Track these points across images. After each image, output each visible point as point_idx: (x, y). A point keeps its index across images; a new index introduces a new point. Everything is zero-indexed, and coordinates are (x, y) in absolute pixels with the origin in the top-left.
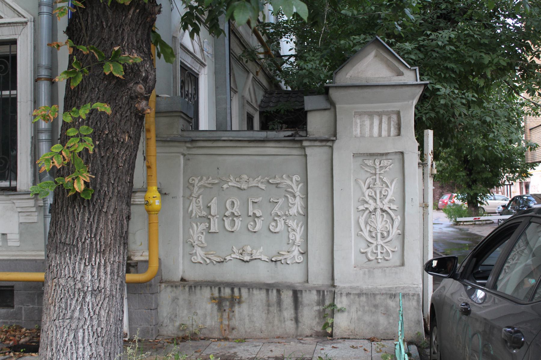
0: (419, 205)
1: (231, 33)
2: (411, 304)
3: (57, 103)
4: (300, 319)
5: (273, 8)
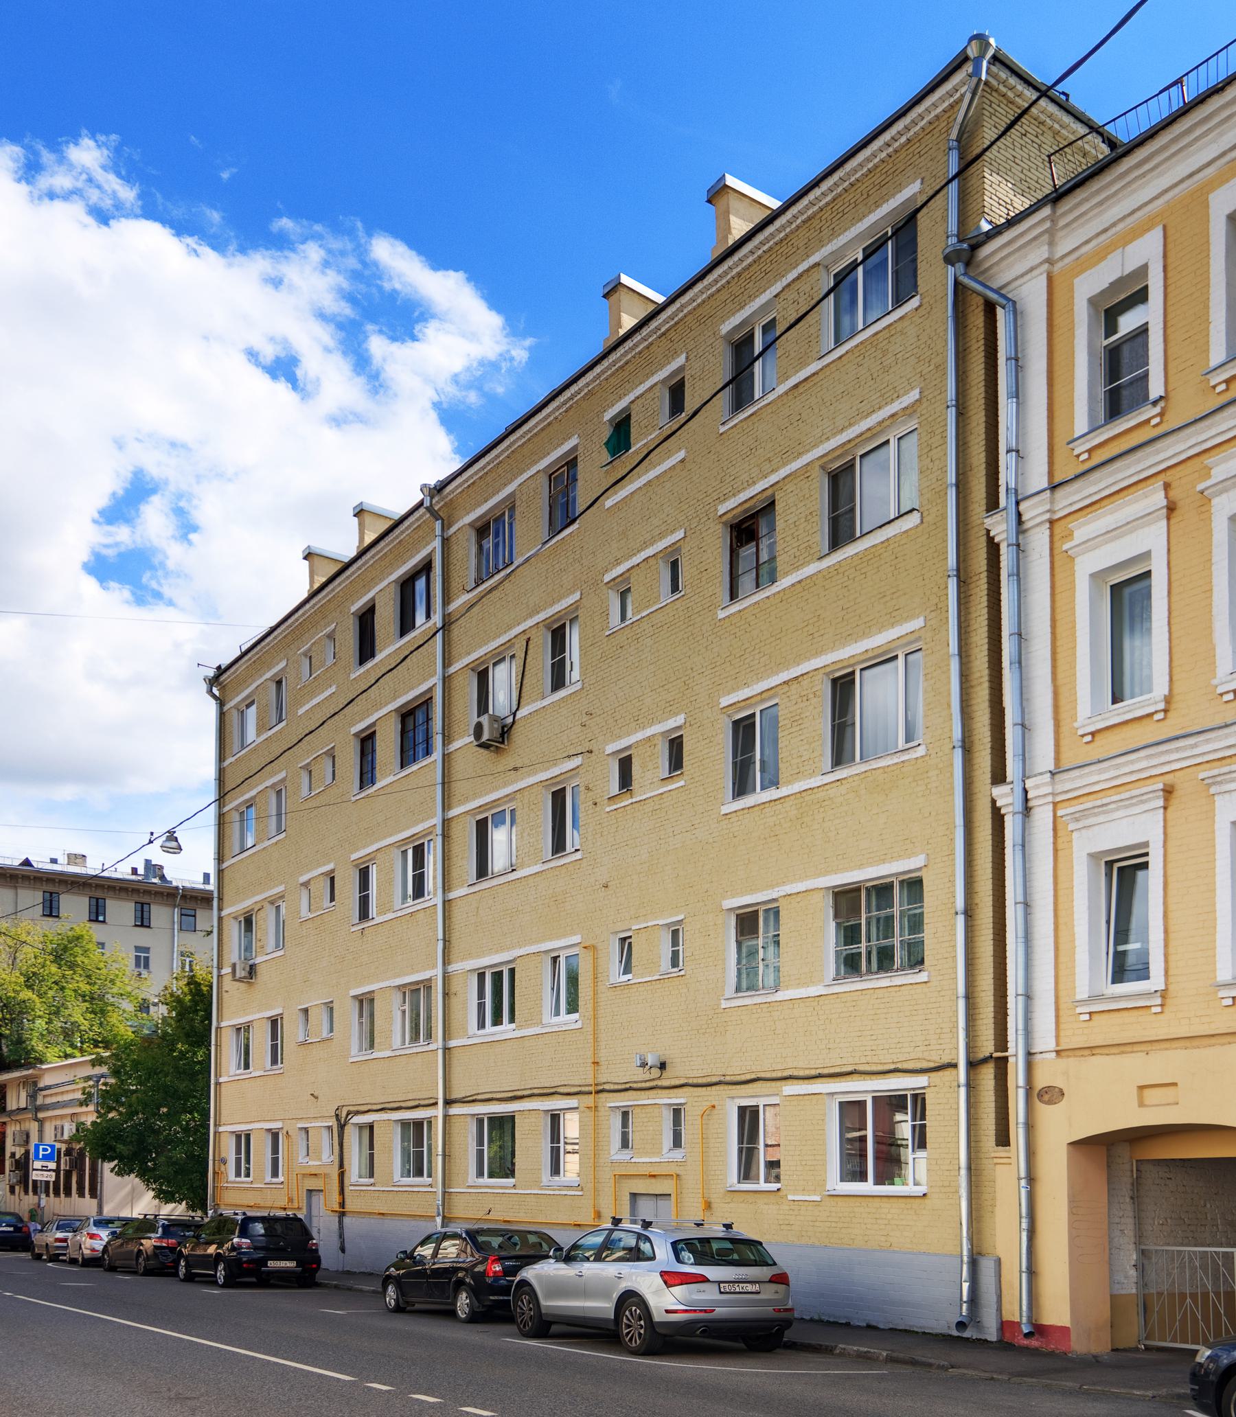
0: (84, 556)
1: (970, 157)
2: (1010, 809)
3: (696, 1263)
4: (1066, 204)
5: (456, 1298)
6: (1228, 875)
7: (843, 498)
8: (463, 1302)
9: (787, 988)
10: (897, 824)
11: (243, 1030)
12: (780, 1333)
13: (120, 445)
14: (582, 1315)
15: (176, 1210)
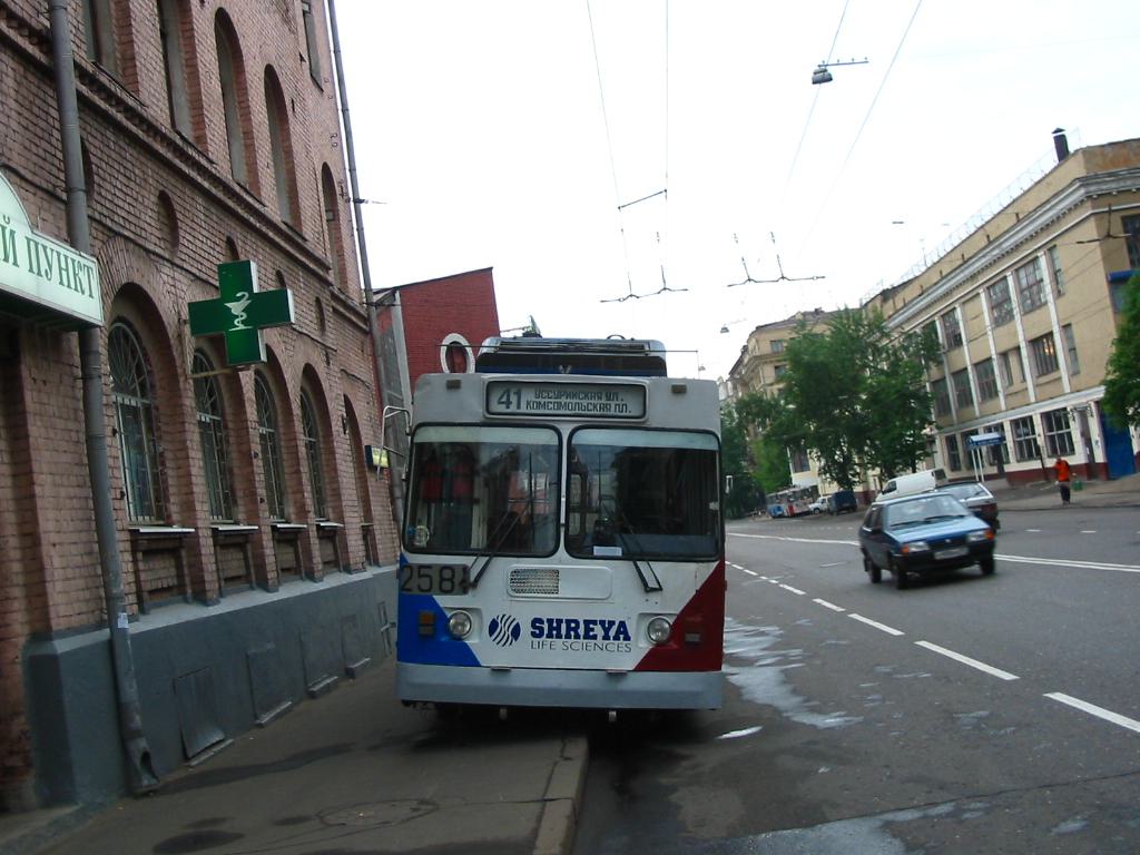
0: (462, 385)
6: (1003, 672)
7: (284, 175)
8: (146, 503)
9: (392, 572)
10: (949, 475)
11: (372, 558)
12: (934, 360)
13: (1077, 129)
14: (70, 313)
15: (1063, 458)
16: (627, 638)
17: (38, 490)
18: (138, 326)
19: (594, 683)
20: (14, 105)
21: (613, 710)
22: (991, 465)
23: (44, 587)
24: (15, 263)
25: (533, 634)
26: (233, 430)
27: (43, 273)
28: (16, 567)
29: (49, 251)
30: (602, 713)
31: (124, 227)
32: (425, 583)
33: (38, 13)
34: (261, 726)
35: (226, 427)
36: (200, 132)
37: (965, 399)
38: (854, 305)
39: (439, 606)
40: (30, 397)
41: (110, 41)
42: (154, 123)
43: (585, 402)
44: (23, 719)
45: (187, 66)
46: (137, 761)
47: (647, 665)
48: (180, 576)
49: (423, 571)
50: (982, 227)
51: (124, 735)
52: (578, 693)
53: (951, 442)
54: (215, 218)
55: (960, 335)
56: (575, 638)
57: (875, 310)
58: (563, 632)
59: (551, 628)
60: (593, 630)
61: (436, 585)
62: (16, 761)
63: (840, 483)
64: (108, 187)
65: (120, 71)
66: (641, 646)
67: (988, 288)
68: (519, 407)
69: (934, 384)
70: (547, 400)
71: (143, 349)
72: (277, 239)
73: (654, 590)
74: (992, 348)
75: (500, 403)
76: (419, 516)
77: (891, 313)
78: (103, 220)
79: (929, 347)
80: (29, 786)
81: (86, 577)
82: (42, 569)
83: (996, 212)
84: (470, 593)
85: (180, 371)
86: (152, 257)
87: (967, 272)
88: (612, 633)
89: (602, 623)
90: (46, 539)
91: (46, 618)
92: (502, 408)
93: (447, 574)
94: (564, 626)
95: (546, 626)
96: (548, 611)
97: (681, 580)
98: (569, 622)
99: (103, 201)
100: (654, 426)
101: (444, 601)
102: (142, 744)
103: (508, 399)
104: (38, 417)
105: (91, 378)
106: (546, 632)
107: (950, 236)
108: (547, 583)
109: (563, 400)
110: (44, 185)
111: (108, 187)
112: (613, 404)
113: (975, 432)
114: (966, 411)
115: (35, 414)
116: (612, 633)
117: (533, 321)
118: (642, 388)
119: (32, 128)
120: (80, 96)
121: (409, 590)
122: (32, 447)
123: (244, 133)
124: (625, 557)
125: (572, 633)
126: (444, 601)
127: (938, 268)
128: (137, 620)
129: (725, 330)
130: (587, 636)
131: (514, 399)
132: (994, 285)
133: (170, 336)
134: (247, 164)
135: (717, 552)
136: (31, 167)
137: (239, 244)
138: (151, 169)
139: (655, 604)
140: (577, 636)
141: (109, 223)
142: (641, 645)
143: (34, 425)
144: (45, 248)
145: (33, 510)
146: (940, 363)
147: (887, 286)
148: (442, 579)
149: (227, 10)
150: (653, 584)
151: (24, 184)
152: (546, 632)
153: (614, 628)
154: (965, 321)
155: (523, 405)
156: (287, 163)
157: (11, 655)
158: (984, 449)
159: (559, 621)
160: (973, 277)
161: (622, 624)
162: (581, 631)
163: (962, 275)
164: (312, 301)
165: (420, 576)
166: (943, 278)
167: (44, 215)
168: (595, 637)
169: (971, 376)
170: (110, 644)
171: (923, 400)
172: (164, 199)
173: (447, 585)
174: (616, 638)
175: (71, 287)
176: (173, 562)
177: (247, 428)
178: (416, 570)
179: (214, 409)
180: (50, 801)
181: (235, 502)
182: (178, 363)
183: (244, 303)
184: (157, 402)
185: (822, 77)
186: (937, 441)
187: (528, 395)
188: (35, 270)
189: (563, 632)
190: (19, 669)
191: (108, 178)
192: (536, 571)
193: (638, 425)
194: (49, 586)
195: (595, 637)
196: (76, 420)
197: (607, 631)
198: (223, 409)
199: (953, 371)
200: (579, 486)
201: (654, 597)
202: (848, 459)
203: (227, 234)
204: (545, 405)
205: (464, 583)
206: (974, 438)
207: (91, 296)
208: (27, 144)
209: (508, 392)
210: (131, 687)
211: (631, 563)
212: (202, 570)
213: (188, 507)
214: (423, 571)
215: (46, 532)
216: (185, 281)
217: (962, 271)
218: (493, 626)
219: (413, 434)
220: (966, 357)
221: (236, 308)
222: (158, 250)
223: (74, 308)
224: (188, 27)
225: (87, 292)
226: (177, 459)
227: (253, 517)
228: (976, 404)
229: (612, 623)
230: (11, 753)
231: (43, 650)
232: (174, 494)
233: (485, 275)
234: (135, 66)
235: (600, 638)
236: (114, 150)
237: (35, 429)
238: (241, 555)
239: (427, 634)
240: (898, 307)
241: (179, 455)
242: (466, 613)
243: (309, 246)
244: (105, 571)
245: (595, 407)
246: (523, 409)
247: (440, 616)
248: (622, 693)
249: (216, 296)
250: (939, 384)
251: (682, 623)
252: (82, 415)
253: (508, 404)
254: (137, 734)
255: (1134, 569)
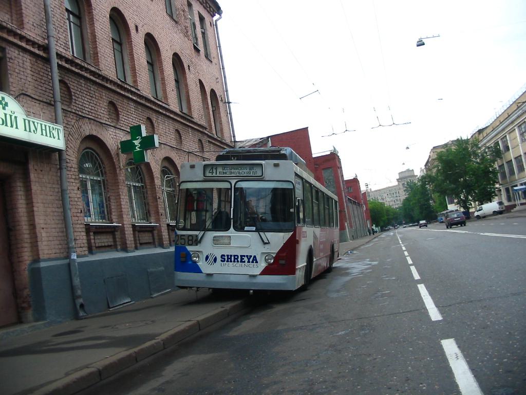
0: (196, 167)
16: (257, 262)
17: (35, 209)
18: (94, 147)
19: (245, 279)
20: (29, 72)
21: (252, 290)
22: (523, 199)
23: (37, 244)
24: (17, 128)
25: (222, 261)
26: (150, 189)
27: (32, 130)
28: (26, 236)
29: (36, 124)
30: (247, 291)
31: (88, 115)
32: (183, 241)
33: (44, 39)
34: (152, 298)
35: (146, 187)
36: (163, 82)
37: (512, 172)
38: (466, 134)
39: (187, 250)
40: (33, 176)
41: (88, 47)
42: (106, 76)
43: (241, 171)
44: (27, 290)
45: (130, 55)
46: (78, 307)
47: (264, 273)
48: (115, 241)
49: (182, 237)
50: (515, 102)
51: (74, 297)
52: (244, 283)
53: (507, 190)
54: (140, 110)
55: (508, 146)
56: (256, 263)
57: (475, 138)
58: (233, 260)
59: (228, 258)
60: (244, 259)
61: (187, 242)
62: (25, 305)
63: (464, 208)
64: (80, 100)
65: (92, 58)
66: (263, 265)
67: (519, 126)
68: (216, 174)
69: (500, 166)
70: (226, 171)
71: (101, 159)
72: (175, 117)
73: (267, 243)
74: (521, 151)
75: (210, 173)
76: (187, 217)
77: (481, 139)
78: (77, 112)
79: (497, 153)
80: (30, 314)
81: (59, 240)
82: (36, 237)
83: (520, 95)
84: (199, 245)
85: (117, 166)
86: (104, 125)
87: (510, 120)
88: (251, 260)
89: (247, 256)
90: (38, 227)
91: (38, 255)
92: (210, 175)
93: (190, 238)
94: (233, 258)
95: (226, 258)
96: (227, 252)
97: (278, 239)
98: (235, 256)
99: (77, 106)
100: (267, 179)
101: (189, 248)
102: (81, 301)
103: (212, 171)
104: (37, 183)
105: (62, 169)
106: (226, 260)
107: (503, 107)
108: (226, 241)
109: (233, 171)
110: (45, 100)
111: (80, 100)
112: (251, 171)
113: (516, 186)
114: (512, 177)
115: (35, 182)
116: (251, 260)
117: (334, 148)
118: (261, 165)
119: (38, 80)
120: (59, 66)
121: (178, 244)
122: (33, 193)
123: (162, 79)
124: (256, 231)
125: (236, 260)
126: (189, 248)
127: (499, 119)
128: (87, 257)
129: (408, 148)
130: (241, 261)
131: (214, 171)
132: (520, 125)
133: (112, 154)
134: (163, 90)
135: (294, 230)
136: (39, 94)
137: (154, 120)
138: (104, 93)
139: (267, 249)
140: (238, 261)
141: (80, 113)
142: (262, 265)
143: (35, 186)
144: (34, 122)
145: (33, 216)
146: (501, 158)
147: (480, 128)
148: (189, 240)
149: (152, 33)
150: (266, 241)
151: (33, 100)
152: (226, 260)
153: (252, 258)
154: (511, 140)
155: (218, 173)
156: (186, 89)
157: (23, 267)
158: (520, 192)
159: (231, 256)
160: (512, 122)
161: (255, 257)
162: (239, 259)
163: (508, 122)
164: (196, 140)
165: (181, 239)
166: (501, 123)
167: (44, 111)
168: (244, 262)
169: (513, 163)
170: (69, 265)
171: (494, 172)
172: (111, 103)
173: (190, 242)
174: (253, 262)
175: (51, 136)
176: (111, 236)
177: (155, 188)
178: (180, 237)
179: (142, 180)
180: (37, 320)
181: (150, 216)
182: (116, 163)
183: (139, 141)
184: (107, 178)
185: (421, 44)
186: (502, 190)
187: (220, 170)
188: (28, 129)
189: (233, 260)
190: (27, 272)
191: (80, 97)
192: (222, 236)
193: (261, 179)
194: (39, 243)
195: (244, 262)
196: (58, 184)
197: (249, 259)
198: (145, 181)
199: (507, 161)
200: (217, 204)
201: (267, 246)
202: (467, 198)
203: (147, 116)
204: (226, 173)
205: (196, 241)
206: (515, 188)
207: (59, 139)
208: (36, 86)
209: (212, 168)
210: (77, 280)
211: (257, 233)
212: (126, 239)
213: (120, 217)
214: (182, 237)
215: (38, 224)
216: (122, 133)
217: (508, 120)
218: (207, 258)
219: (179, 186)
220: (512, 155)
221: (137, 142)
222: (107, 123)
223: (42, 142)
224: (130, 40)
225: (57, 137)
226: (116, 199)
227: (158, 221)
228: (516, 174)
229: (251, 256)
230: (24, 302)
231: (36, 266)
232: (114, 212)
233: (305, 130)
234: (98, 56)
235: (246, 262)
236: (84, 87)
237: (35, 187)
238: (151, 235)
239: (185, 262)
240: (484, 136)
241: (117, 197)
242: (198, 254)
243: (195, 120)
244: (68, 238)
245: (245, 173)
246: (218, 175)
247: (188, 253)
248: (255, 283)
249: (129, 138)
250: (501, 166)
251: (278, 257)
252: (59, 182)
253: (212, 173)
254: (79, 297)
255: (523, 237)
